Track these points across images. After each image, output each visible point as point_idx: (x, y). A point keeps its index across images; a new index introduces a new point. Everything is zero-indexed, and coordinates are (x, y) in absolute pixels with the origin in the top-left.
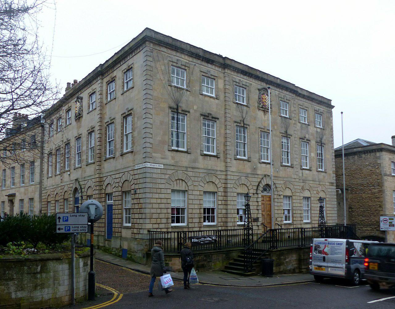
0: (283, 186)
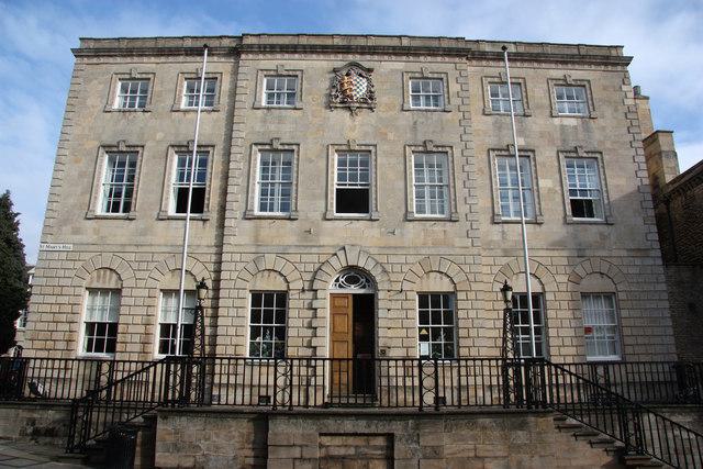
0: (251, 267)
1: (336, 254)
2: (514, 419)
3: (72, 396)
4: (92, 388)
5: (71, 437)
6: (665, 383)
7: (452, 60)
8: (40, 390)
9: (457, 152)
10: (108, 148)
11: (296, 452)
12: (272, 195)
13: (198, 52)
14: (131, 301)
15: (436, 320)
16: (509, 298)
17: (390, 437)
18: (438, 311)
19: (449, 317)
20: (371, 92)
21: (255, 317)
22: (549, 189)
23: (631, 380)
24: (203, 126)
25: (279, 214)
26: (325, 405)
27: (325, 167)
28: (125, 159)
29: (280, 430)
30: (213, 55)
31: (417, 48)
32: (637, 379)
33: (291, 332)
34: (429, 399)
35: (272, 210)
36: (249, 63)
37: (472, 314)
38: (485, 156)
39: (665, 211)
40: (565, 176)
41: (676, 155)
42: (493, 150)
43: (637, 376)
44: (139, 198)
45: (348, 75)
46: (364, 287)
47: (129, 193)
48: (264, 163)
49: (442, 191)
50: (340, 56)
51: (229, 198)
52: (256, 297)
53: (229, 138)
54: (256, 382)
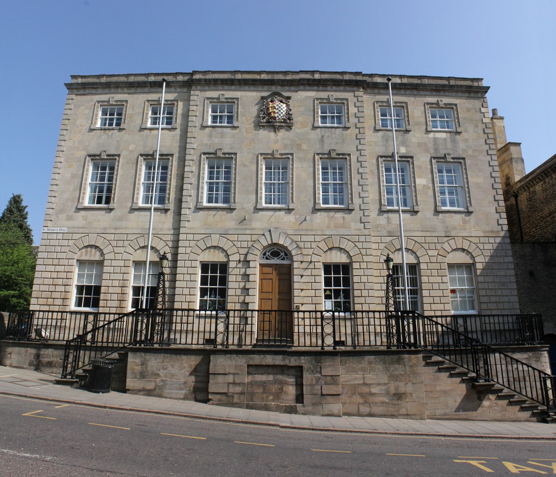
1: (264, 235)
2: (392, 356)
3: (66, 339)
4: (81, 333)
5: (65, 368)
6: (509, 330)
7: (351, 89)
8: (43, 334)
9: (354, 158)
10: (93, 157)
11: (230, 379)
12: (217, 191)
13: (157, 85)
14: (111, 270)
15: (337, 283)
16: (391, 267)
17: (300, 369)
18: (339, 278)
19: (347, 282)
20: (289, 114)
21: (204, 281)
22: (424, 185)
23: (502, 328)
24: (164, 140)
25: (220, 205)
26: (254, 346)
27: (255, 170)
28: (105, 164)
29: (218, 363)
30: (171, 86)
31: (325, 80)
32: (488, 329)
33: (230, 292)
34: (329, 341)
35: (217, 202)
36: (198, 96)
37: (364, 279)
38: (374, 161)
39: (514, 203)
40: (437, 180)
41: (522, 160)
42: (381, 157)
43: (488, 326)
44: (118, 193)
45: (272, 101)
46: (283, 259)
47: (109, 190)
48: (211, 167)
49: (340, 189)
50: (266, 88)
51: (185, 193)
52: (205, 267)
53: (183, 149)
54: (202, 329)
